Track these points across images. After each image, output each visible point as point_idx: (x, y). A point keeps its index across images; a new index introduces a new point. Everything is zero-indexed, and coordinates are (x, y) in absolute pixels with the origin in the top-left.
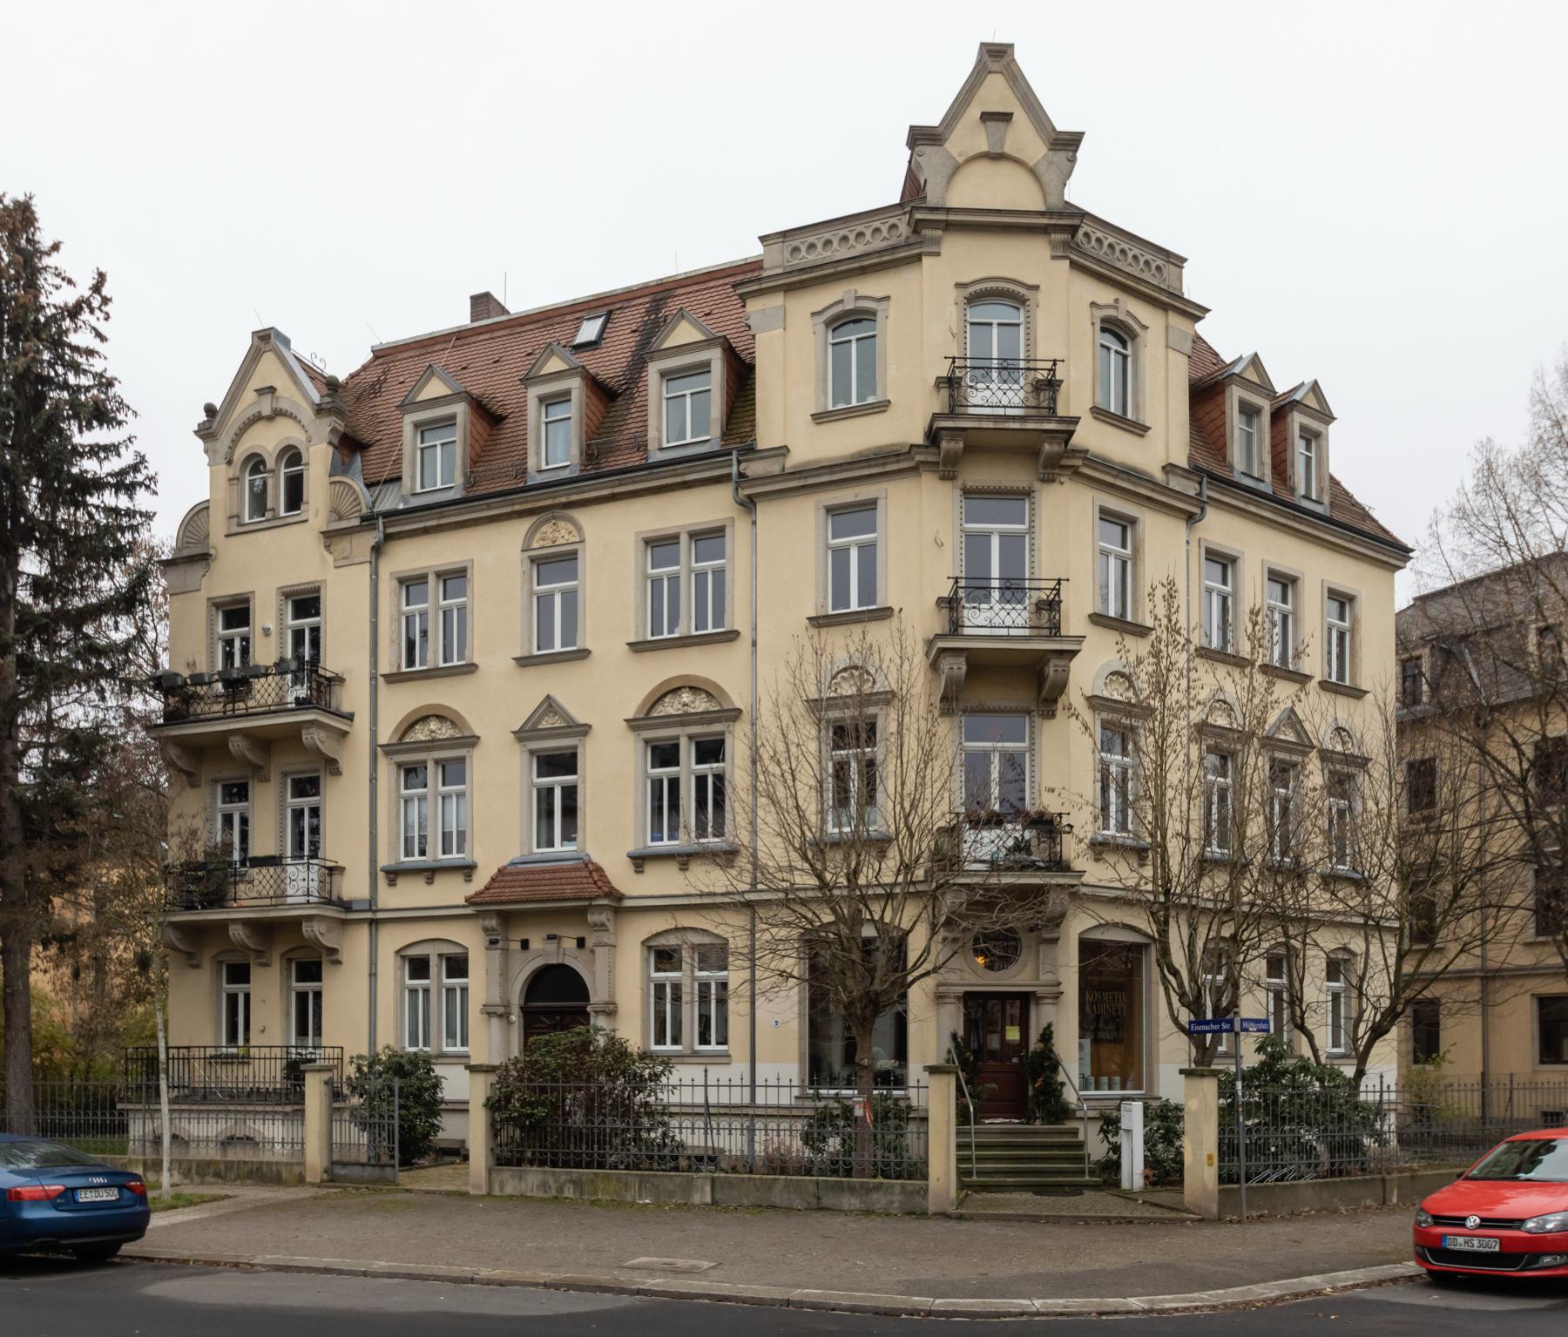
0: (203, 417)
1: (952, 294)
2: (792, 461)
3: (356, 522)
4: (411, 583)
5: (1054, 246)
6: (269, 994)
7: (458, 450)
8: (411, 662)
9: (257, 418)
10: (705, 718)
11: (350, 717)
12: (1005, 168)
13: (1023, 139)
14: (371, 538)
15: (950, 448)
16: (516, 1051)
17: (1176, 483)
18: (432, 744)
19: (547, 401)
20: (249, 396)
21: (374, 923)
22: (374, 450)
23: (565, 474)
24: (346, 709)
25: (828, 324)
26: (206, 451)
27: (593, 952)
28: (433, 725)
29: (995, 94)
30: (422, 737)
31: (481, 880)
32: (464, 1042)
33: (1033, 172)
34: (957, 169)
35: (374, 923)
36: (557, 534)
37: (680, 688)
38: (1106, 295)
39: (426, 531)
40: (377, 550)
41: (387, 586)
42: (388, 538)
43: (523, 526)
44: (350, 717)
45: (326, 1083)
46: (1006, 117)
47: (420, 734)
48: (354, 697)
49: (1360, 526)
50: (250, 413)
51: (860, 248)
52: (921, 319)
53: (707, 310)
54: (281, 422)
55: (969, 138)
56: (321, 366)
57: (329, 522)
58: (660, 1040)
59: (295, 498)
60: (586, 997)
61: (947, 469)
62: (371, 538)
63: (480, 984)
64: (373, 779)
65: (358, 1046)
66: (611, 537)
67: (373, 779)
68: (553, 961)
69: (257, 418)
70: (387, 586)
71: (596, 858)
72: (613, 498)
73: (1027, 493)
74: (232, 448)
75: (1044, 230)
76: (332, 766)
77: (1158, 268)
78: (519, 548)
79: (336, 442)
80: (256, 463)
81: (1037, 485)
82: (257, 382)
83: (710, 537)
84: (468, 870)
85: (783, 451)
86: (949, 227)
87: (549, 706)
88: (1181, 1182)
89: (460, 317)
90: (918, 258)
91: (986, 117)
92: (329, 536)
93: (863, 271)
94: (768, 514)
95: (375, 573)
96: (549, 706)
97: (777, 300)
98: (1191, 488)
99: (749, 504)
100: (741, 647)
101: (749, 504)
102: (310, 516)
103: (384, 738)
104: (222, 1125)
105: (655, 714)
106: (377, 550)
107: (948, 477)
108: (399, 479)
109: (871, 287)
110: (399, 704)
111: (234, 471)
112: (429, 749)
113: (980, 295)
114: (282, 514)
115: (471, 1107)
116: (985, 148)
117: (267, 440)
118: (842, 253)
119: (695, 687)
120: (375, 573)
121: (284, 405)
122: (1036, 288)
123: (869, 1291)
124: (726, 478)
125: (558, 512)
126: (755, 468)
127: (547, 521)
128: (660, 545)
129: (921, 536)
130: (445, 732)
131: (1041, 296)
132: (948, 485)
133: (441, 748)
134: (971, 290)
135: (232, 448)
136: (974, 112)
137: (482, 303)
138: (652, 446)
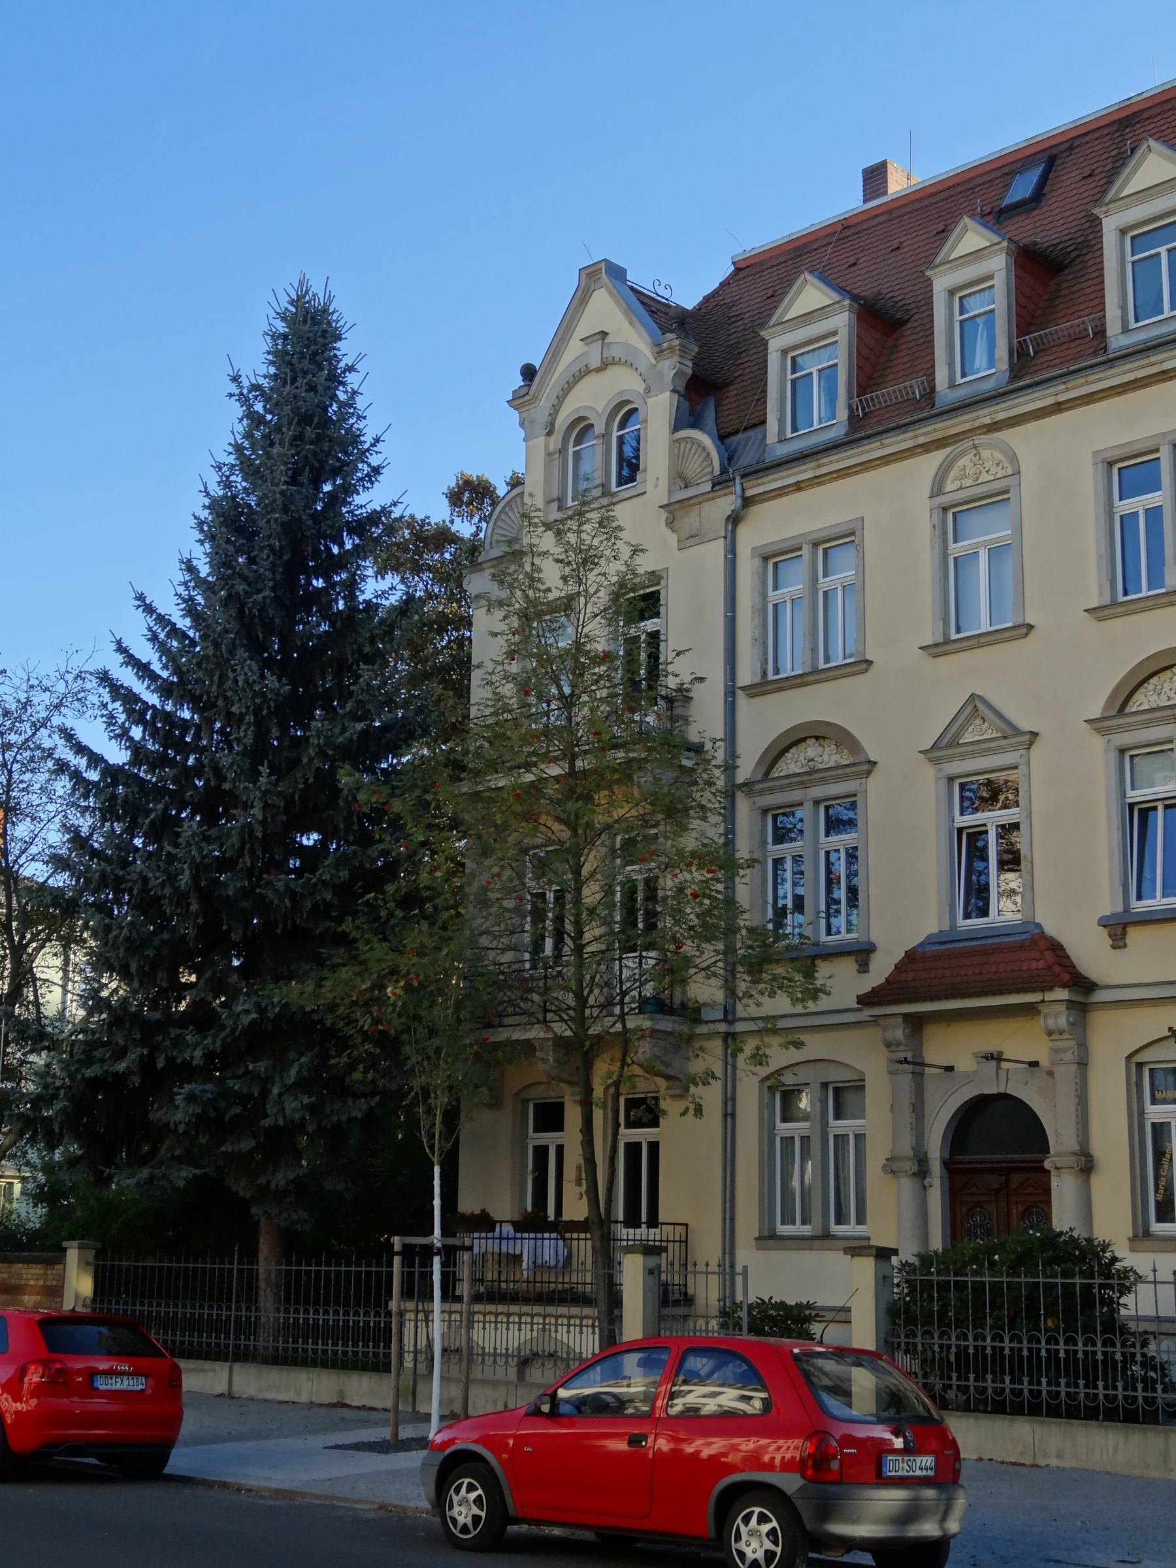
0: (519, 381)
3: (707, 487)
4: (774, 559)
10: (839, 772)
18: (812, 776)
20: (574, 349)
22: (732, 391)
23: (989, 385)
26: (522, 424)
27: (1050, 1074)
28: (811, 750)
30: (795, 768)
31: (881, 969)
32: (861, 1220)
37: (804, 740)
39: (798, 487)
42: (747, 502)
45: (651, 1272)
47: (791, 765)
50: (580, 365)
53: (895, 244)
54: (613, 373)
56: (666, 294)
57: (670, 492)
58: (841, 1219)
59: (630, 469)
60: (1047, 1150)
63: (877, 1124)
68: (992, 1090)
71: (1050, 929)
72: (1059, 408)
78: (927, 491)
79: (682, 390)
80: (581, 429)
82: (585, 328)
84: (863, 954)
87: (975, 706)
96: (975, 706)
102: (649, 487)
103: (744, 774)
104: (527, 1334)
105: (775, 773)
106: (735, 520)
108: (764, 422)
111: (555, 442)
112: (805, 785)
114: (614, 488)
115: (854, 1315)
117: (593, 398)
119: (818, 733)
121: (615, 352)
123: (538, 1523)
125: (979, 439)
127: (963, 453)
130: (829, 756)
133: (823, 781)
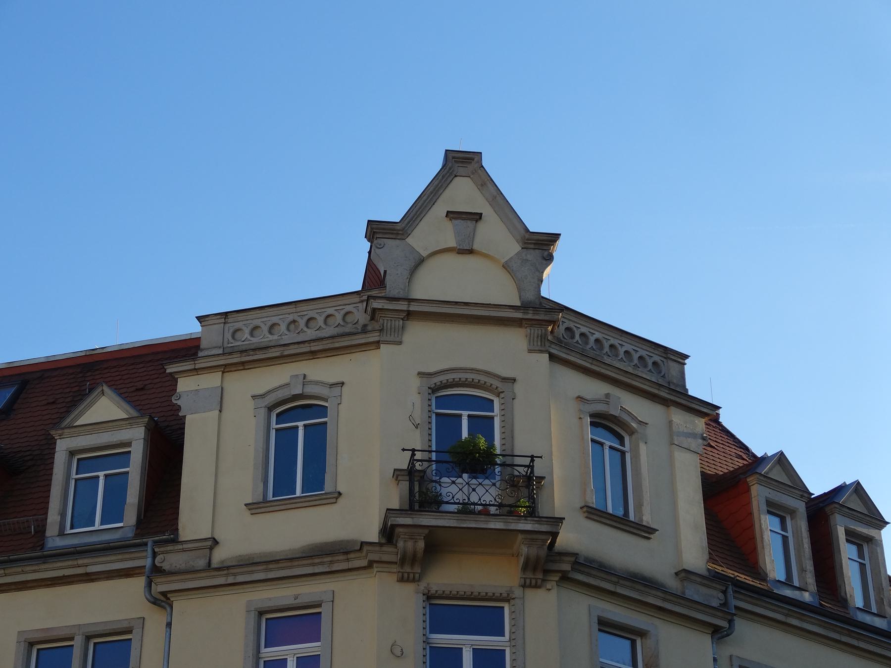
2: (219, 555)
17: (694, 592)
29: (462, 194)
38: (595, 389)
46: (477, 217)
86: (409, 315)
93: (313, 355)
97: (212, 380)
98: (714, 597)
116: (452, 243)
126: (172, 560)
131: (517, 387)
132: (409, 588)
134: (437, 380)
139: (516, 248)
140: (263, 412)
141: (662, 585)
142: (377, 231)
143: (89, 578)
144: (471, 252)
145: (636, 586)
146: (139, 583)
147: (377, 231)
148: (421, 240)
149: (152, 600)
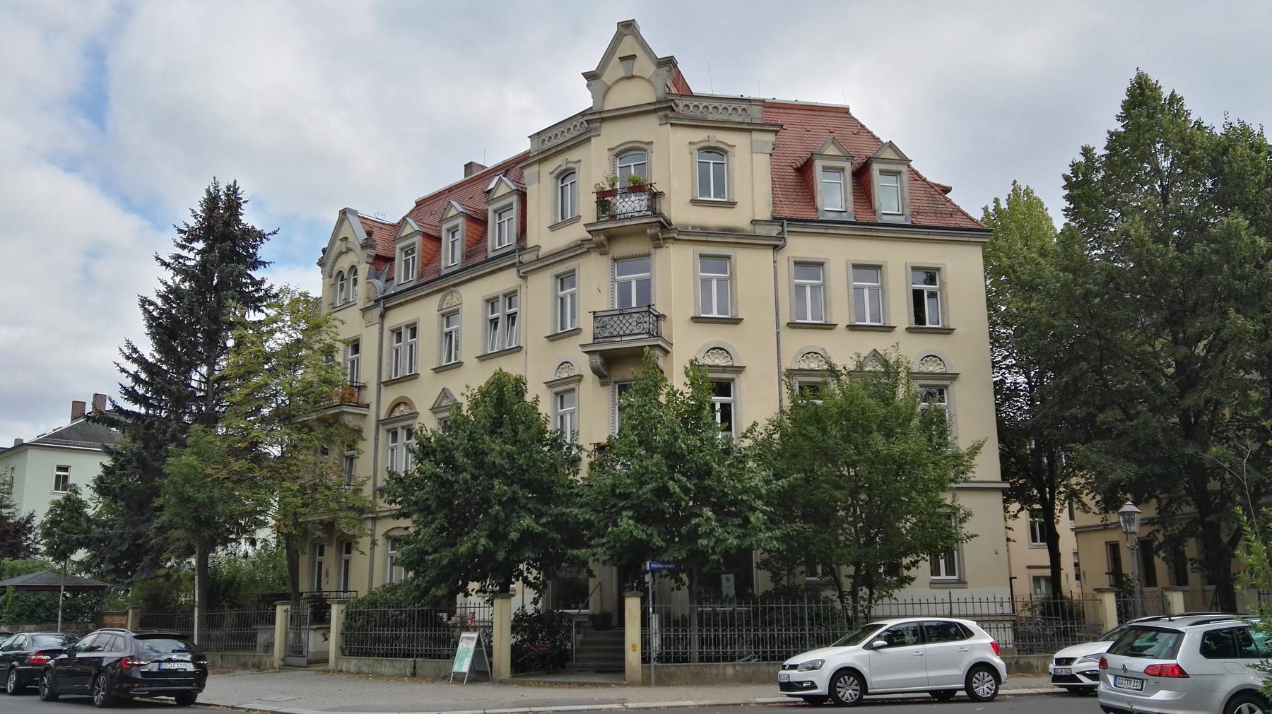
1: (607, 154)
2: (542, 253)
4: (398, 333)
5: (660, 119)
6: (330, 558)
7: (514, 220)
8: (450, 359)
9: (341, 254)
11: (367, 406)
12: (635, 82)
13: (643, 66)
14: (378, 311)
15: (604, 239)
16: (636, 596)
17: (761, 230)
19: (499, 212)
21: (374, 519)
24: (366, 402)
25: (557, 178)
29: (628, 47)
33: (649, 81)
34: (609, 88)
35: (374, 519)
36: (451, 301)
38: (700, 136)
39: (401, 304)
40: (382, 316)
41: (387, 334)
42: (386, 309)
43: (438, 297)
44: (367, 406)
46: (633, 57)
48: (370, 396)
49: (952, 222)
51: (569, 136)
52: (595, 165)
55: (616, 70)
61: (601, 249)
62: (378, 311)
64: (377, 439)
65: (363, 593)
66: (472, 297)
67: (377, 439)
69: (341, 254)
70: (387, 334)
73: (648, 255)
74: (332, 270)
75: (655, 111)
76: (359, 431)
77: (744, 110)
81: (653, 251)
83: (510, 296)
85: (538, 247)
86: (603, 120)
88: (623, 671)
89: (460, 176)
90: (589, 139)
91: (622, 59)
92: (364, 310)
93: (569, 148)
94: (534, 280)
95: (382, 328)
97: (535, 168)
98: (774, 230)
99: (524, 277)
100: (522, 354)
101: (524, 277)
106: (382, 316)
107: (602, 254)
109: (573, 156)
110: (390, 396)
111: (332, 281)
113: (621, 153)
116: (623, 75)
117: (344, 264)
118: (554, 142)
120: (382, 328)
121: (350, 246)
122: (651, 143)
124: (513, 265)
126: (526, 258)
128: (491, 302)
129: (596, 285)
131: (654, 147)
132: (605, 258)
135: (332, 270)
136: (616, 59)
137: (469, 167)
138: (489, 250)
139: (653, 68)
140: (554, 180)
141: (742, 230)
142: (590, 76)
143: (502, 269)
144: (633, 77)
145: (731, 236)
146: (514, 271)
147: (590, 76)
148: (607, 78)
149: (128, 352)
